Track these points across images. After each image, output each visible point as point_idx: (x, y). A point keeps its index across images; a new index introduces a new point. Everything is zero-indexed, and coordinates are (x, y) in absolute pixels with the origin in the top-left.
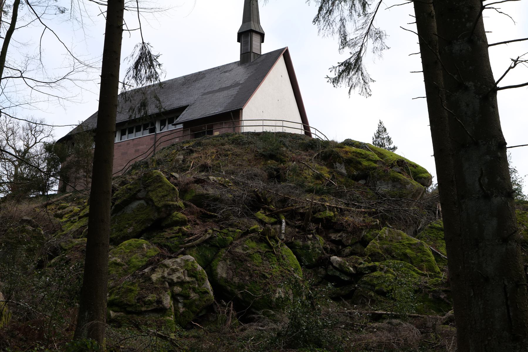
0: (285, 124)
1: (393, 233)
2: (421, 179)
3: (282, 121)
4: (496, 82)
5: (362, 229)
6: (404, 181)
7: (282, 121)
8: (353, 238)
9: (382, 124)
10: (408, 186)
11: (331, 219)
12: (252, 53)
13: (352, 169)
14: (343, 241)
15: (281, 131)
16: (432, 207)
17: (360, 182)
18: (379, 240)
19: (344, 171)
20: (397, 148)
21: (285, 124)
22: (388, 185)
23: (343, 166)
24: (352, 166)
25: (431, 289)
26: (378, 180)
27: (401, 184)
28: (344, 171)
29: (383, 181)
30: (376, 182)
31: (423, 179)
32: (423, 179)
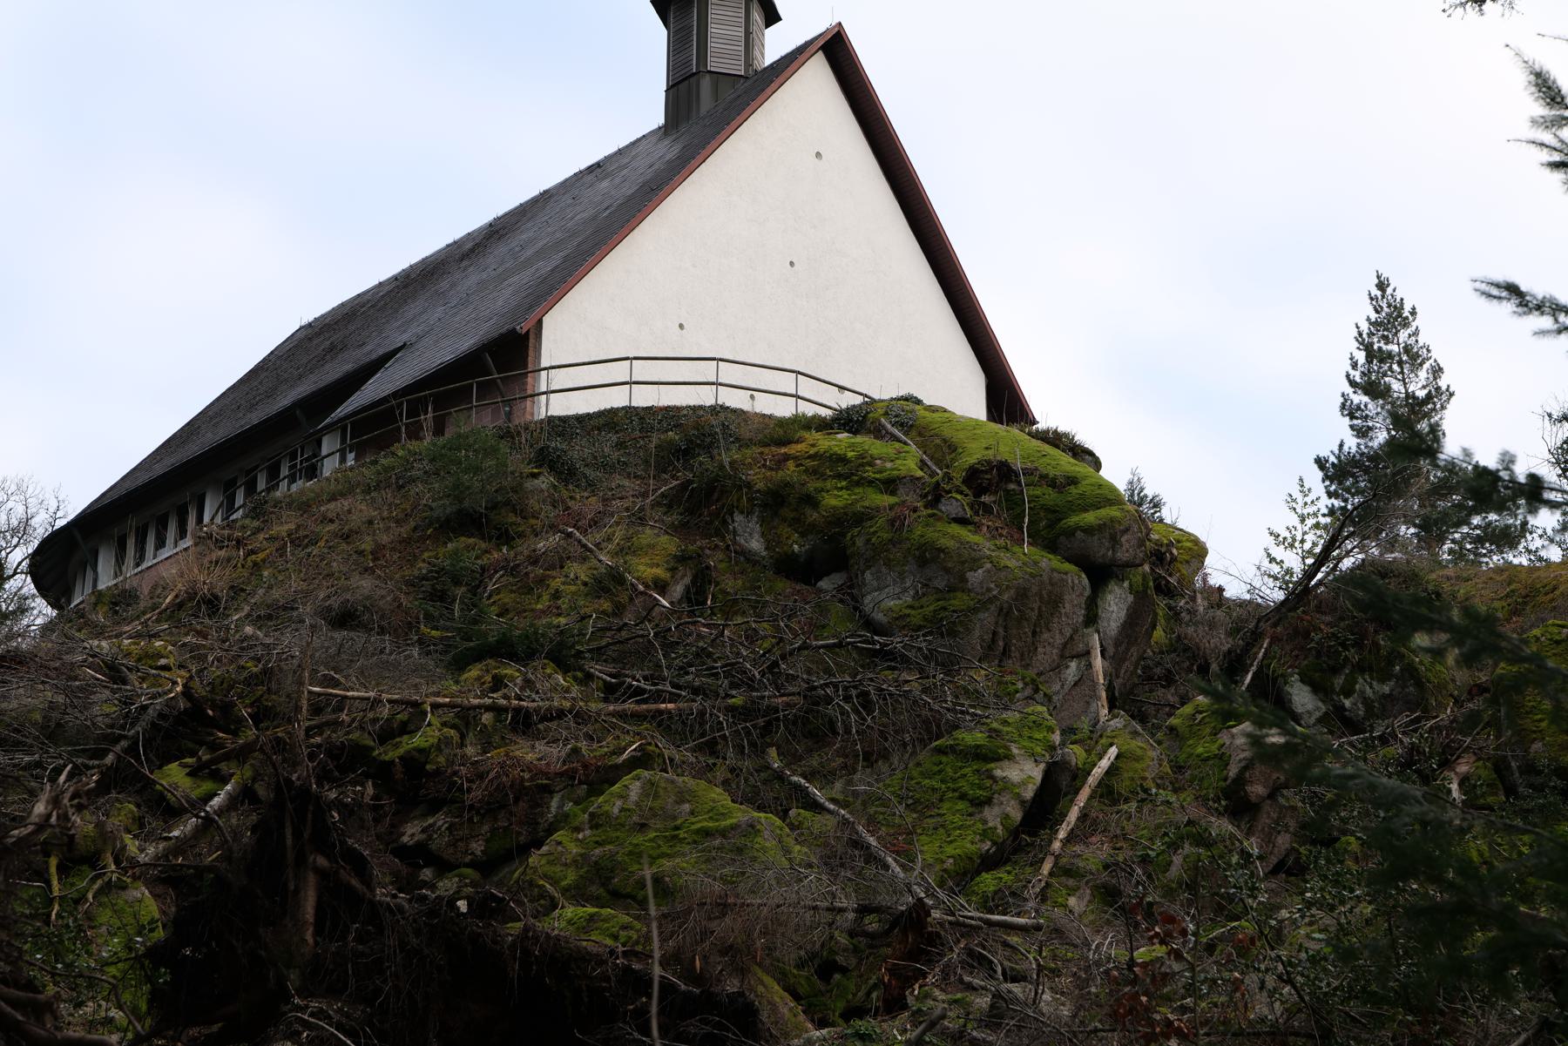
0: (642, 371)
1: (661, 792)
2: (1074, 535)
3: (714, 359)
4: (769, 59)
5: (548, 790)
6: (960, 555)
7: (714, 359)
8: (493, 830)
9: (1389, 291)
10: (975, 577)
11: (426, 763)
12: (708, 77)
13: (785, 530)
14: (433, 847)
15: (710, 402)
16: (36, 656)
17: (824, 584)
18: (591, 828)
19: (756, 545)
20: (1452, 395)
21: (642, 371)
22: (903, 580)
23: (754, 525)
24: (784, 520)
25: (700, 1020)
26: (869, 567)
27: (947, 570)
28: (756, 545)
29: (884, 569)
30: (863, 573)
31: (1079, 534)
32: (1079, 534)
